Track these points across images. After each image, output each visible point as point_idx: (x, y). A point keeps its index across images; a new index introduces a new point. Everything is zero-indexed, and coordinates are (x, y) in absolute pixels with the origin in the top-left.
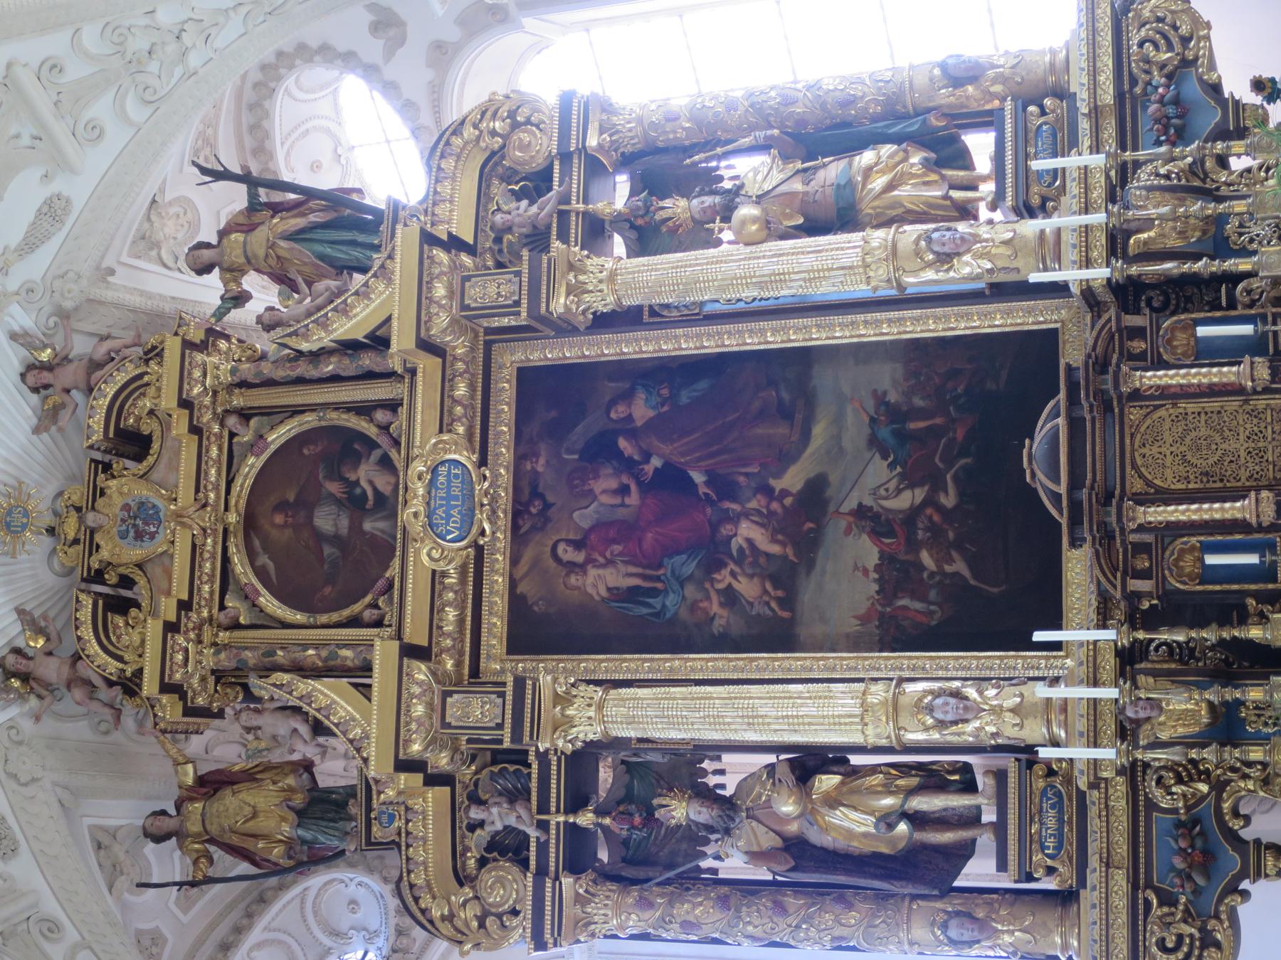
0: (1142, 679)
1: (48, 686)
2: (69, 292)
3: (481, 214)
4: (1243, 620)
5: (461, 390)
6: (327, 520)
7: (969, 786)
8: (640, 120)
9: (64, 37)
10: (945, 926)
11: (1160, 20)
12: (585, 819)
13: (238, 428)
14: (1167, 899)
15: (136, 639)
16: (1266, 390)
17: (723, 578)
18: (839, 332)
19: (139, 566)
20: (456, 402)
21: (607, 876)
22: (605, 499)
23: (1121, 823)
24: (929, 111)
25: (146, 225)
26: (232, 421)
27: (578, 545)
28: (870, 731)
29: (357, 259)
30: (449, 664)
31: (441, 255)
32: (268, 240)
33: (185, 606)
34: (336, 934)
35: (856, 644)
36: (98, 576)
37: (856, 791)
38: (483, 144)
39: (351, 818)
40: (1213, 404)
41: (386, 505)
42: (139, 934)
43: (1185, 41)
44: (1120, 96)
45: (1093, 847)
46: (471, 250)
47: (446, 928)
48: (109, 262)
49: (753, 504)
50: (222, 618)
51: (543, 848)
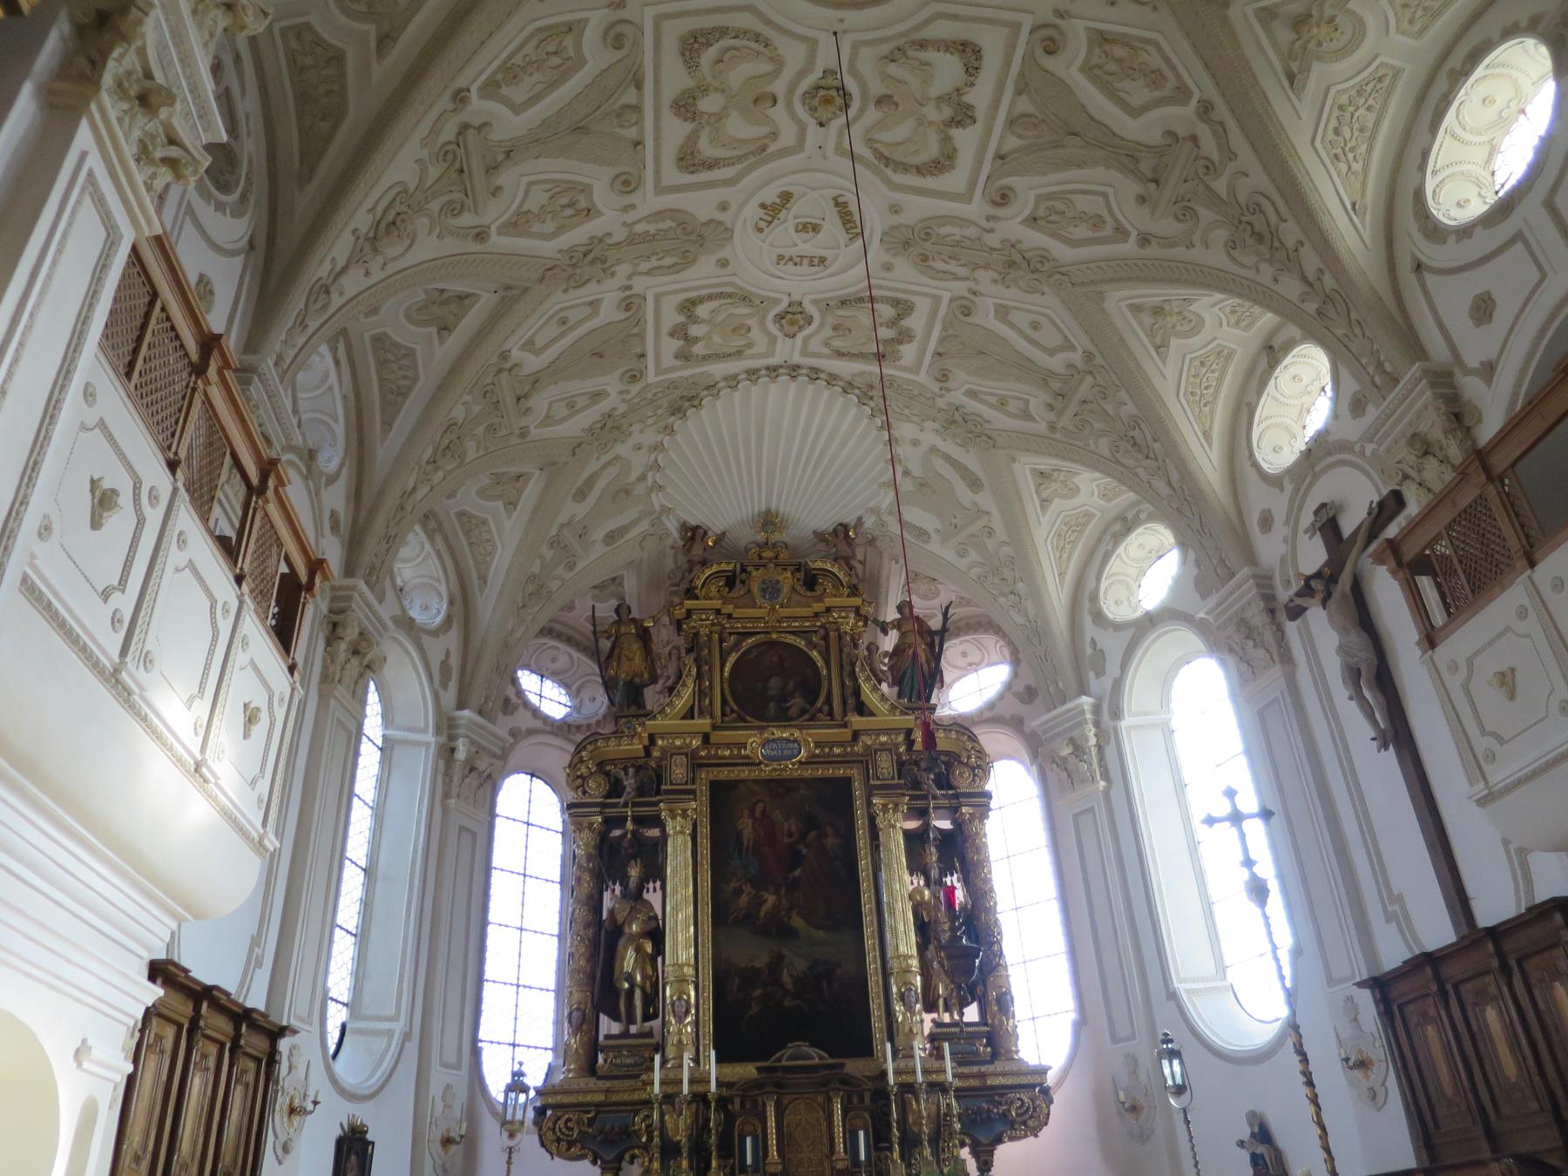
0: (694, 1106)
1: (689, 550)
4: (720, 1157)
5: (837, 751)
6: (775, 683)
7: (647, 1017)
8: (977, 833)
9: (1006, 539)
10: (578, 1009)
11: (1035, 1110)
12: (630, 825)
13: (819, 635)
14: (591, 1122)
15: (712, 595)
16: (833, 1168)
17: (747, 888)
18: (870, 942)
19: (749, 591)
20: (831, 748)
21: (603, 837)
22: (786, 826)
23: (626, 1097)
24: (985, 986)
26: (822, 632)
27: (764, 813)
28: (670, 968)
30: (703, 754)
33: (730, 616)
34: (578, 691)
35: (716, 958)
36: (743, 570)
37: (644, 961)
39: (629, 707)
40: (826, 1140)
41: (783, 717)
42: (573, 602)
43: (1024, 1123)
44: (993, 1088)
45: (616, 1083)
47: (576, 759)
49: (784, 901)
50: (725, 635)
51: (615, 805)
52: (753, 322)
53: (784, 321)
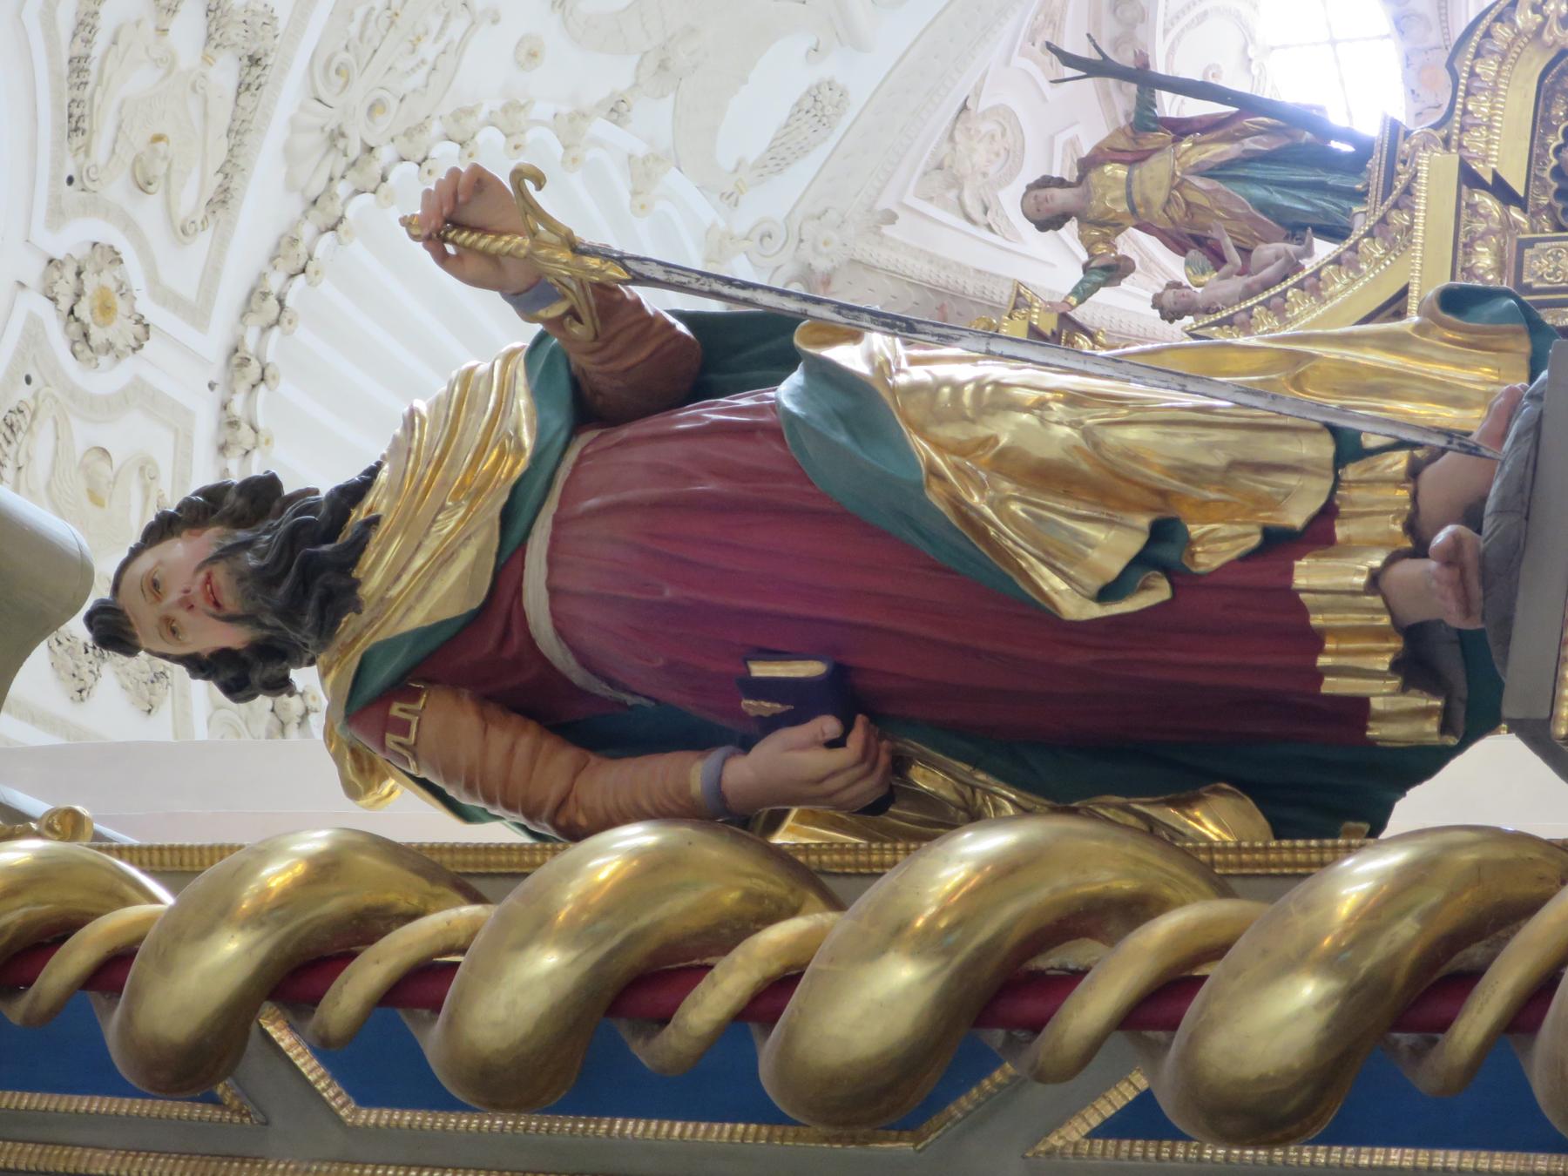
2: (826, 244)
3: (1536, 151)
25: (946, 148)
29: (1326, 212)
31: (1487, 202)
32: (1174, 175)
38: (1547, 38)
46: (1521, 203)
48: (886, 202)
52: (83, 435)
53: (97, 335)
